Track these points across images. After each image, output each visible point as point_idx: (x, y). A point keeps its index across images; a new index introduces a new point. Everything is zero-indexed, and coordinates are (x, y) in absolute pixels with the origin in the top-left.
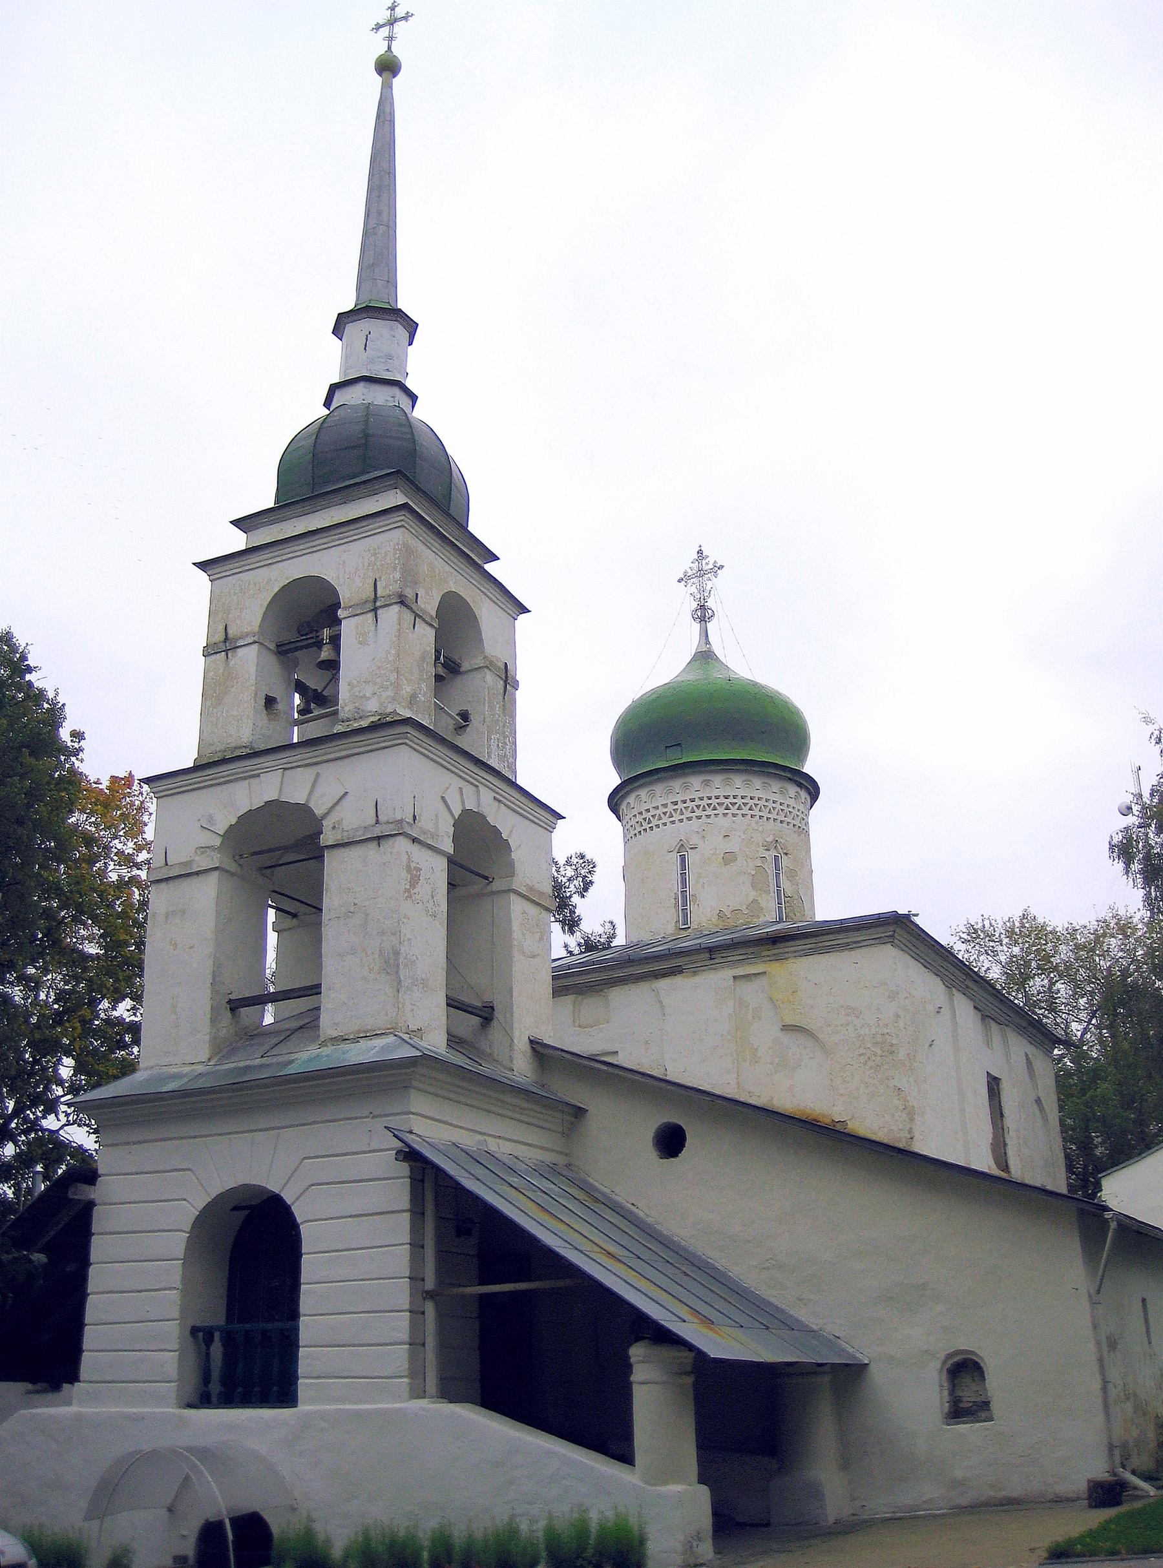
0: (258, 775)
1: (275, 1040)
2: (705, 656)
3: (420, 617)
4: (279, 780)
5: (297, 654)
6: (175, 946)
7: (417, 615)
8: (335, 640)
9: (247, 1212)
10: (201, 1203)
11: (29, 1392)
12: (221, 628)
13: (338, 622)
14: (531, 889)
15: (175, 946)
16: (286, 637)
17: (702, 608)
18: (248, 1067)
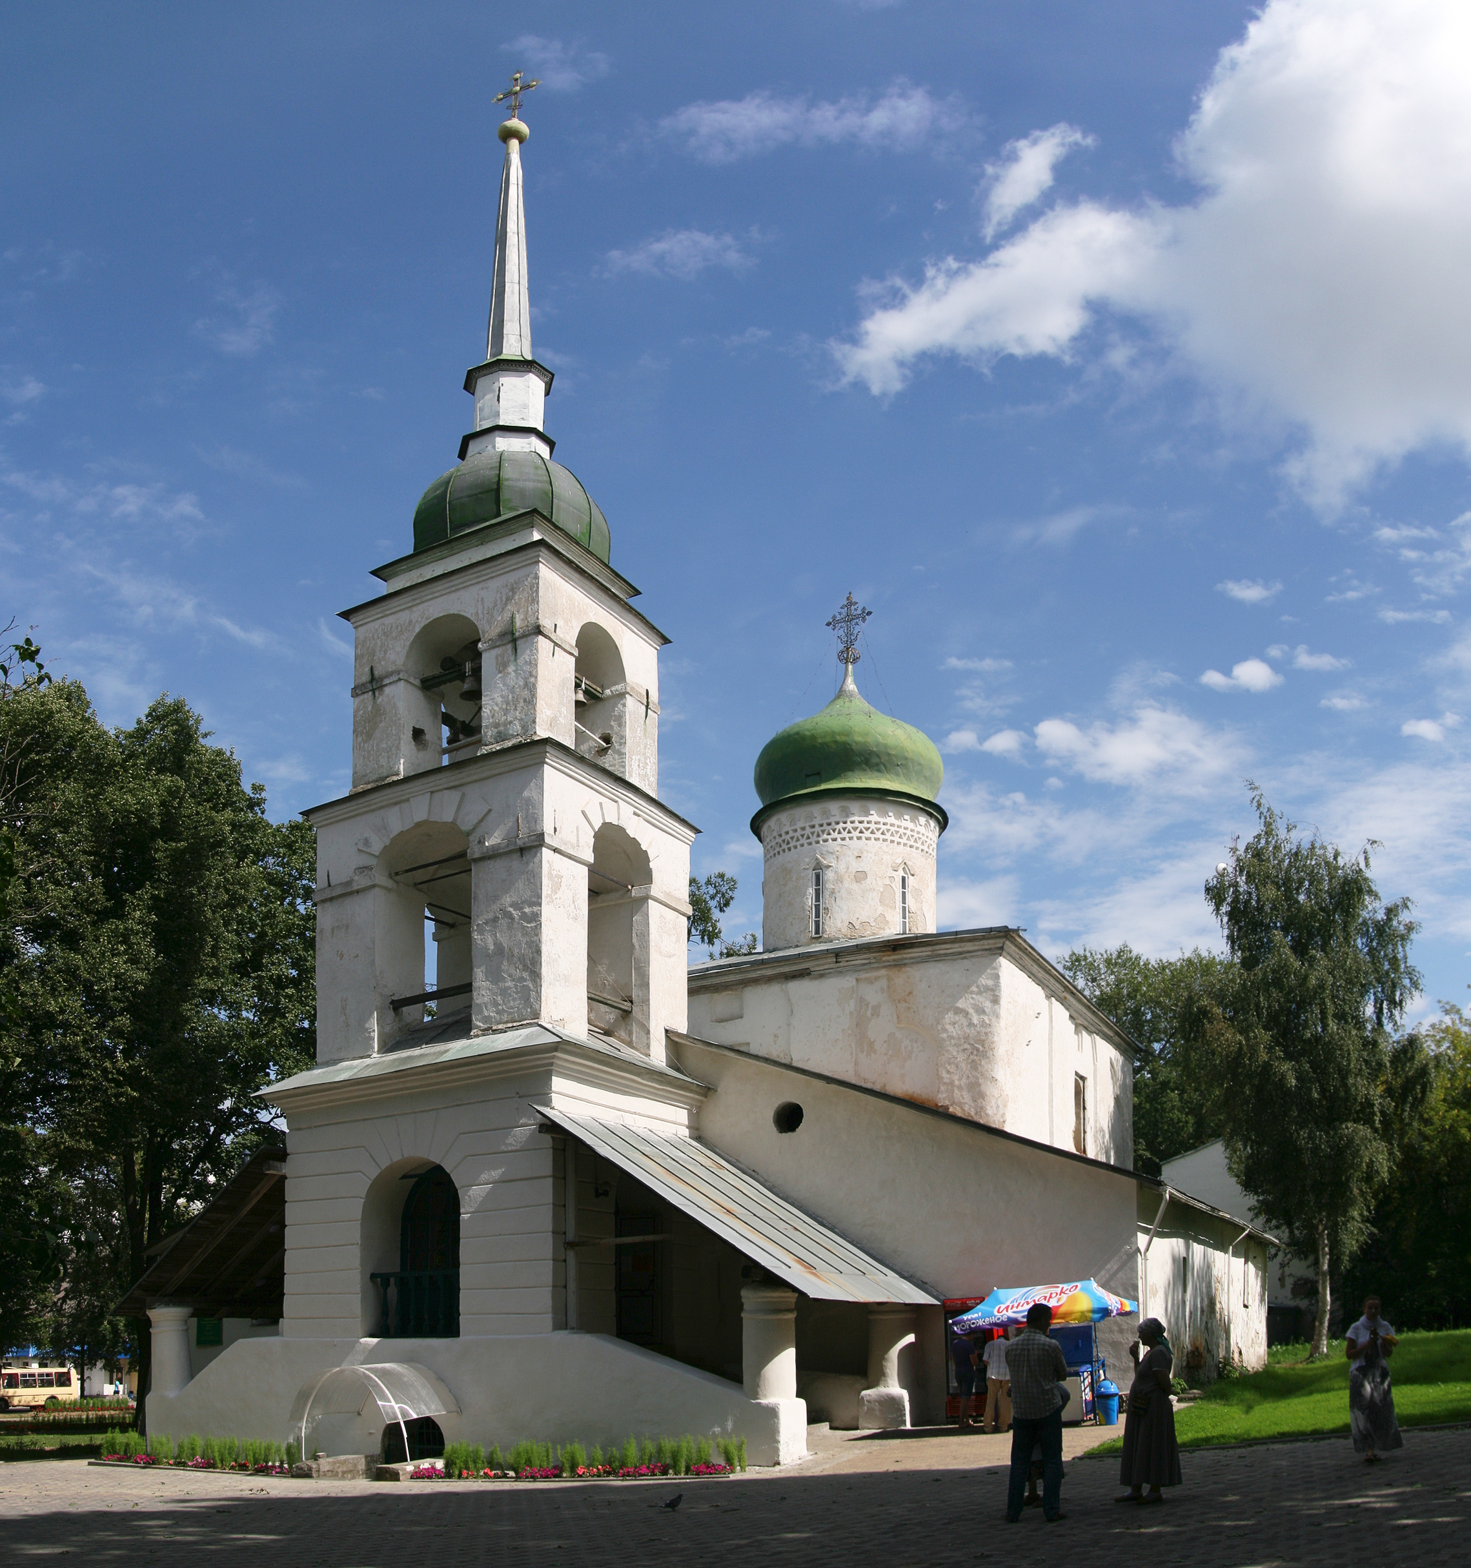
0: (408, 800)
1: (434, 1034)
3: (559, 646)
5: (442, 687)
6: (342, 956)
7: (556, 644)
8: (477, 672)
9: (415, 1180)
10: (374, 1173)
11: (252, 1325)
12: (367, 669)
13: (479, 655)
14: (668, 894)
15: (342, 956)
16: (429, 673)
18: (409, 1057)
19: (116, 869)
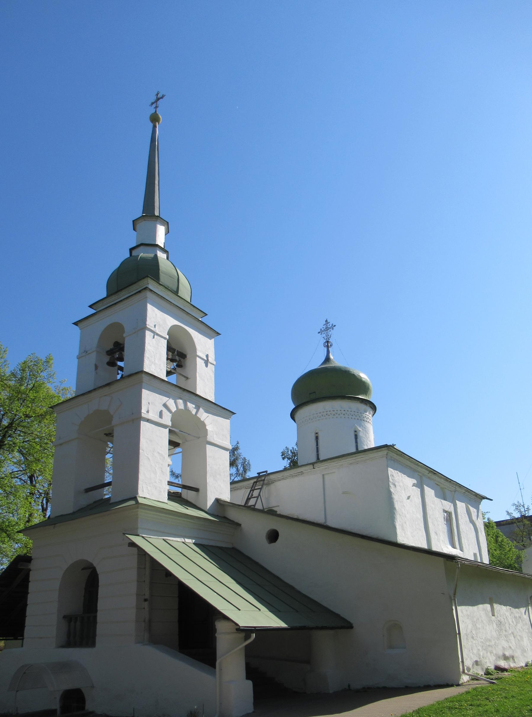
2: (327, 359)
4: (321, 452)
17: (328, 342)
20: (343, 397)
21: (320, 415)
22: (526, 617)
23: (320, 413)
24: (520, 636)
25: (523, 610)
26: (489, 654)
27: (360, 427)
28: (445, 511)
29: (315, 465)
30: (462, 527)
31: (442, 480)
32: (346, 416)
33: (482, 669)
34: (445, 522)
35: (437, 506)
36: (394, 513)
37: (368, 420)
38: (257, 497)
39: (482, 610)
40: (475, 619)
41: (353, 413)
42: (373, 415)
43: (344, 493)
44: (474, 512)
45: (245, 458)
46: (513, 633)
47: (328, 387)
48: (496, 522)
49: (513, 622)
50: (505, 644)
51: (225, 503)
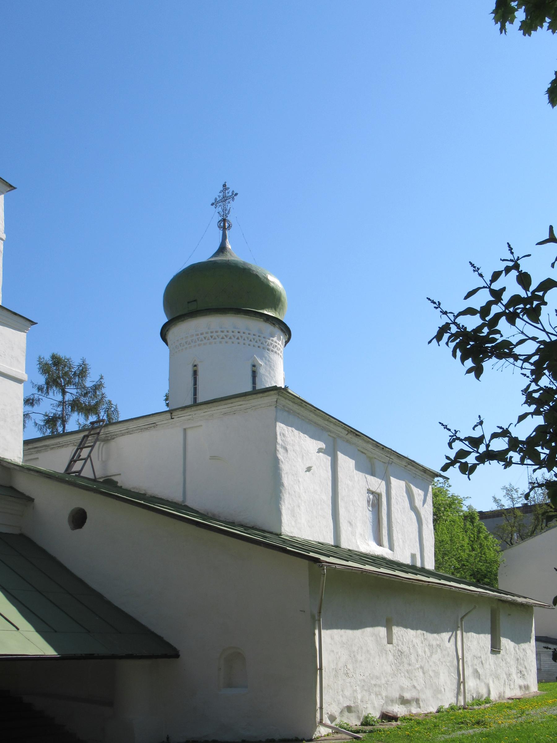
2: (222, 249)
11: (501, 501)
17: (224, 220)
19: (553, 444)
20: (238, 311)
21: (202, 337)
22: (450, 646)
23: (202, 334)
24: (434, 671)
25: (446, 636)
26: (373, 696)
27: (262, 359)
28: (370, 491)
29: (174, 414)
30: (395, 515)
31: (370, 446)
32: (241, 341)
33: (359, 718)
34: (370, 508)
35: (356, 483)
36: (281, 492)
37: (275, 350)
38: (86, 460)
39: (371, 637)
40: (355, 649)
41: (251, 337)
42: (287, 342)
43: (213, 458)
44: (419, 495)
45: (110, 402)
46: (422, 667)
47: (219, 292)
48: (480, 512)
49: (425, 652)
50: (406, 683)
51: (16, 467)
